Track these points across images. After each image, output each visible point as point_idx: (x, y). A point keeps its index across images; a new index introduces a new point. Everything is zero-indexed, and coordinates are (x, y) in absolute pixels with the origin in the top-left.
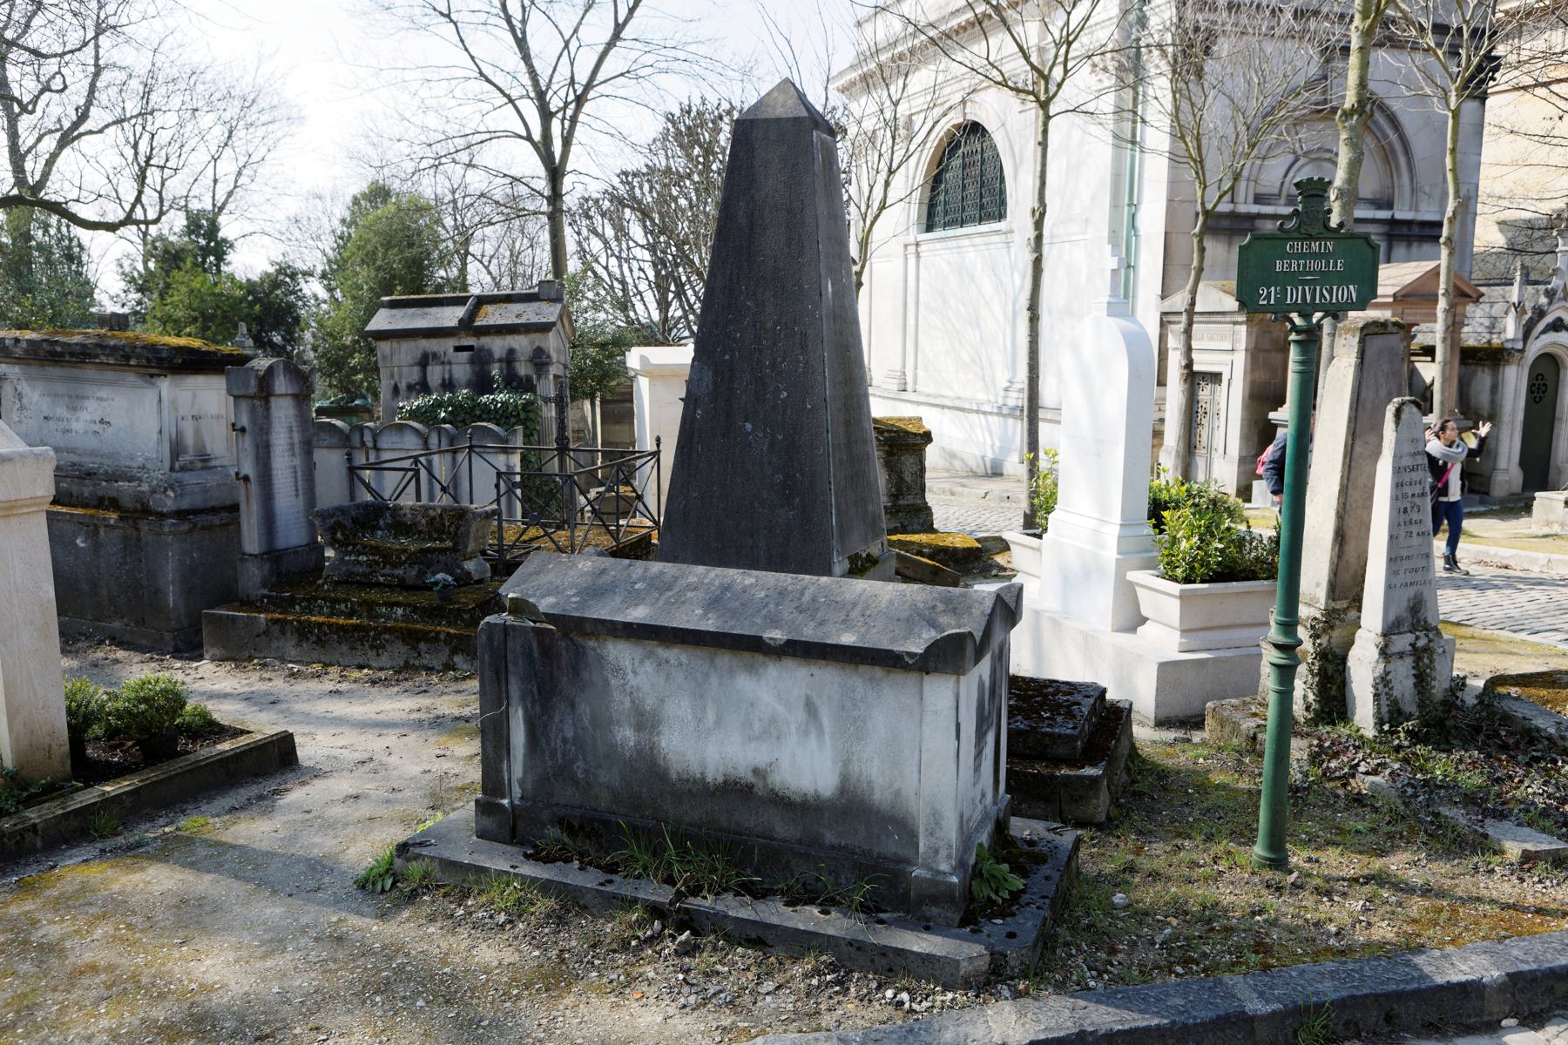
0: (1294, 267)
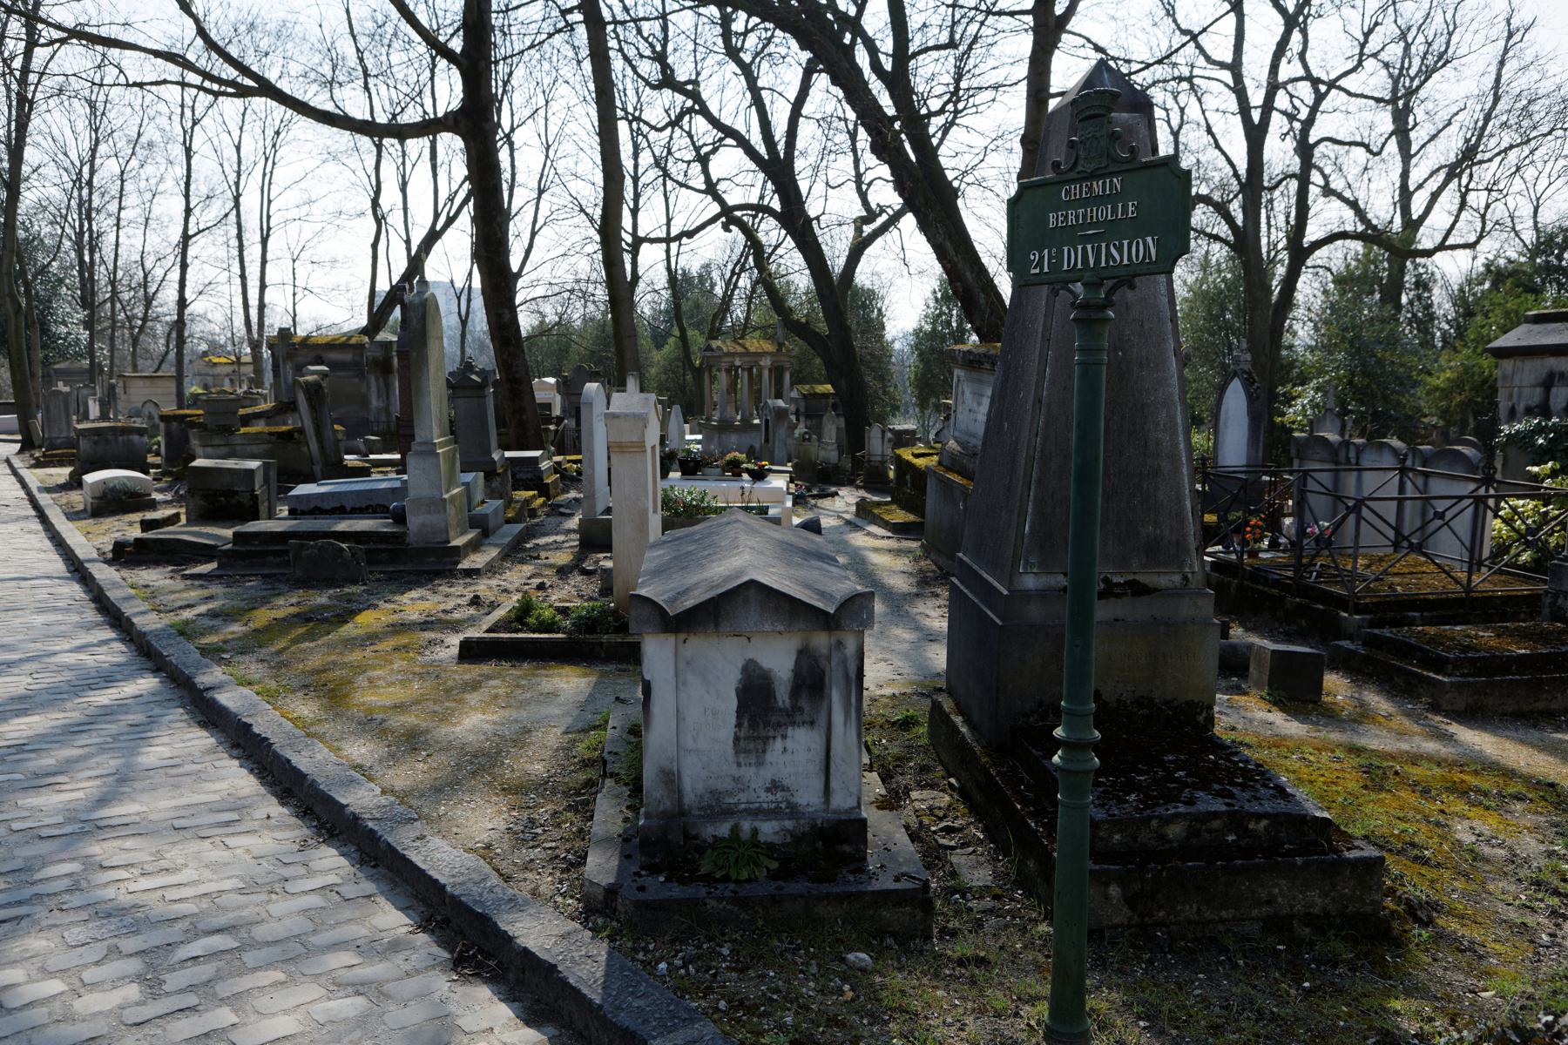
0: (1071, 220)
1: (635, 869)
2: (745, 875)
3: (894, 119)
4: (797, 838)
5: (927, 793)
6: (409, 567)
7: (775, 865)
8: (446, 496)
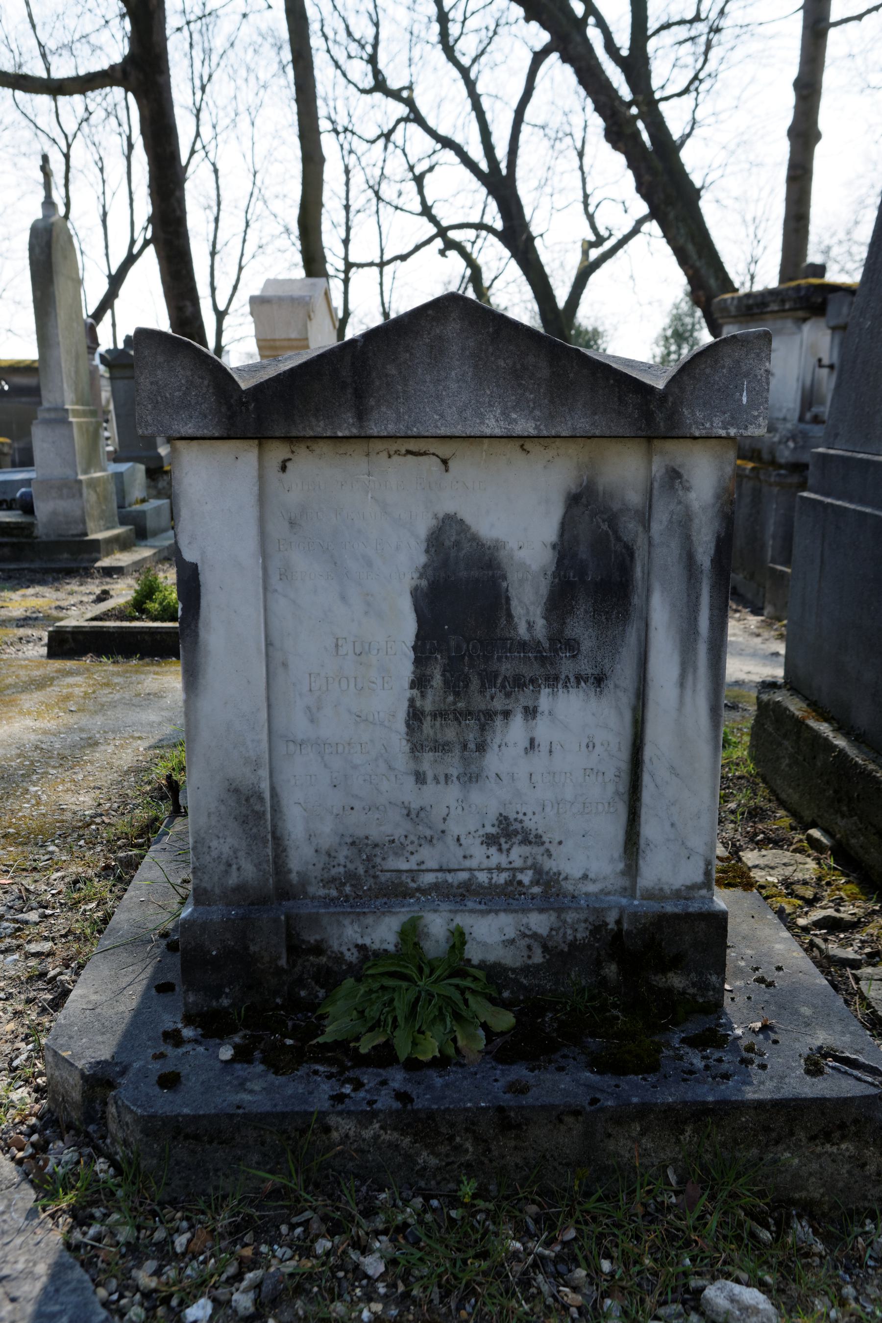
1: (171, 1021)
2: (430, 1048)
3: (630, 104)
4: (559, 956)
5: (771, 855)
6: (36, 565)
7: (504, 1020)
8: (81, 477)
